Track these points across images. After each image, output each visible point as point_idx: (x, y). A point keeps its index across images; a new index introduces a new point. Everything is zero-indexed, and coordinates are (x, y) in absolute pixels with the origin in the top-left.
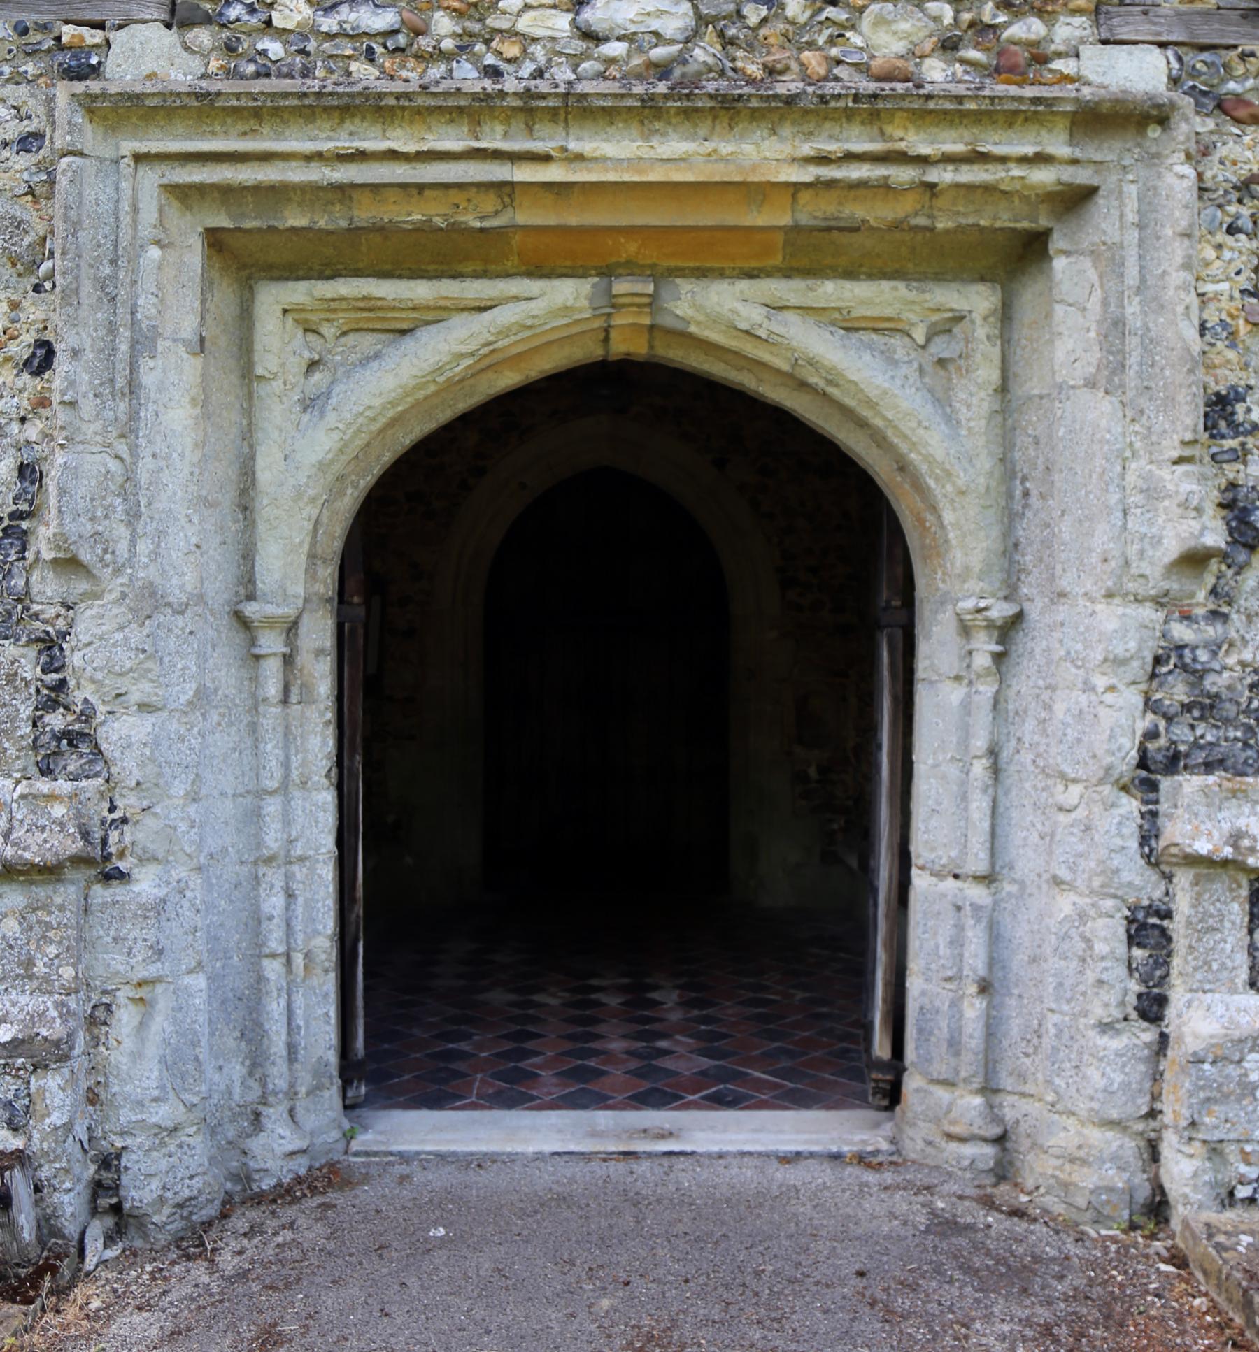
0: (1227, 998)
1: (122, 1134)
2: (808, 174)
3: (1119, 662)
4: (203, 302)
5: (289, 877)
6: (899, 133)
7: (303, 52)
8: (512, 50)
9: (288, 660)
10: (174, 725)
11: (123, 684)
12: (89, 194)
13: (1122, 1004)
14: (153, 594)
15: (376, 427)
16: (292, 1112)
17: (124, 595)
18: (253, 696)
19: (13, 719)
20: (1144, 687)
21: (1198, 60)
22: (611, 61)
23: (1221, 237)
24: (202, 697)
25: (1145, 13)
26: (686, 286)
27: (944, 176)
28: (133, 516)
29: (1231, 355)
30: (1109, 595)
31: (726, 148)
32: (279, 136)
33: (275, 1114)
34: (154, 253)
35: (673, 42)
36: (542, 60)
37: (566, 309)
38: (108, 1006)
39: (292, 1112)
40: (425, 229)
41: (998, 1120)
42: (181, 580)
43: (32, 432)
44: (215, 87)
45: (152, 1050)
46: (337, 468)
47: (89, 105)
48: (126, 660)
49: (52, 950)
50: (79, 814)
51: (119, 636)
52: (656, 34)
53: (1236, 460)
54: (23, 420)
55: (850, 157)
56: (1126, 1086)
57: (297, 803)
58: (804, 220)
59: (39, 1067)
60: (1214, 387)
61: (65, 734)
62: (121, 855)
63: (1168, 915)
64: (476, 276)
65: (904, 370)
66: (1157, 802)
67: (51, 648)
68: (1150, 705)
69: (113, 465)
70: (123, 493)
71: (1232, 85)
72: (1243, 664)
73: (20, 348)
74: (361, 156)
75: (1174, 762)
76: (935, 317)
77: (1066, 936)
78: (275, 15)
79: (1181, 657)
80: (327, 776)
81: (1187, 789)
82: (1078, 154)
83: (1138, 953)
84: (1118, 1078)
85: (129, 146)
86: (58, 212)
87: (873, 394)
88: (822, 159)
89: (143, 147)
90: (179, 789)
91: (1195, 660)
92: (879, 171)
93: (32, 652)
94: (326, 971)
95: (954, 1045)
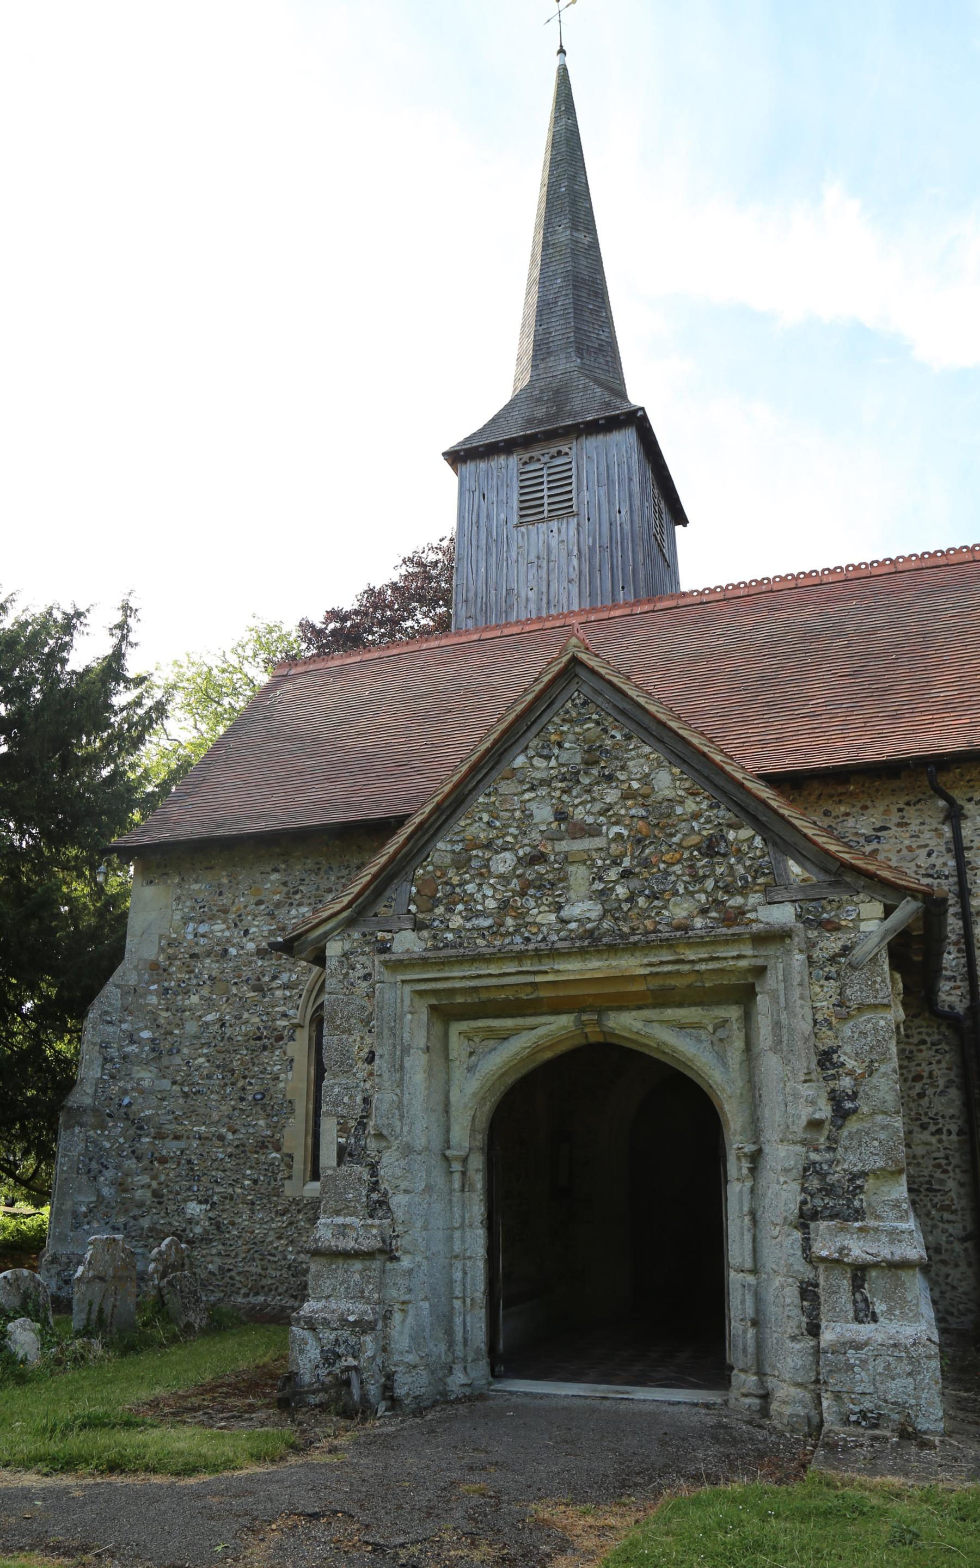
0: (843, 1325)
1: (395, 1365)
2: (647, 971)
3: (786, 1171)
4: (428, 1033)
5: (464, 1265)
6: (682, 951)
7: (459, 937)
8: (535, 930)
9: (464, 1173)
10: (417, 1199)
11: (398, 1182)
12: (386, 996)
13: (799, 1327)
14: (409, 1147)
15: (495, 1078)
16: (465, 1368)
17: (398, 1148)
18: (450, 1188)
19: (360, 1195)
20: (800, 1181)
21: (810, 906)
22: (571, 931)
23: (822, 982)
24: (429, 1188)
25: (786, 888)
26: (612, 1014)
27: (703, 967)
28: (402, 1117)
29: (829, 1033)
30: (782, 1141)
31: (614, 963)
32: (451, 971)
33: (457, 1367)
34: (409, 1016)
35: (595, 921)
36: (545, 932)
37: (564, 1027)
38: (391, 1311)
39: (465, 1368)
40: (506, 1000)
41: (765, 1388)
42: (420, 1142)
43: (368, 1086)
44: (429, 954)
45: (407, 1331)
46: (481, 1094)
47: (385, 963)
48: (399, 1173)
49: (371, 1287)
50: (382, 1233)
51: (397, 1163)
52: (588, 918)
53: (835, 1079)
54: (365, 1081)
55: (662, 963)
56: (804, 1366)
57: (468, 1233)
58: (651, 987)
59: (364, 1332)
60: (821, 1048)
61: (378, 1201)
62: (397, 1250)
63: (817, 1285)
64: (531, 1015)
65: (705, 1044)
66: (809, 1233)
67: (373, 1168)
68: (804, 1190)
69: (395, 1098)
70: (398, 1108)
71: (825, 915)
72: (845, 1170)
73: (364, 1054)
74: (479, 976)
75: (815, 1215)
76: (716, 1021)
77: (777, 1296)
78: (450, 924)
79: (815, 1168)
80: (482, 1223)
81: (821, 1227)
82: (756, 953)
83: (805, 1303)
84: (800, 1363)
85: (400, 978)
86: (375, 1003)
87: (690, 1056)
88: (651, 965)
89: (404, 978)
90: (419, 1224)
91: (821, 1169)
92: (676, 967)
93: (367, 1169)
94: (481, 1308)
95: (745, 1350)
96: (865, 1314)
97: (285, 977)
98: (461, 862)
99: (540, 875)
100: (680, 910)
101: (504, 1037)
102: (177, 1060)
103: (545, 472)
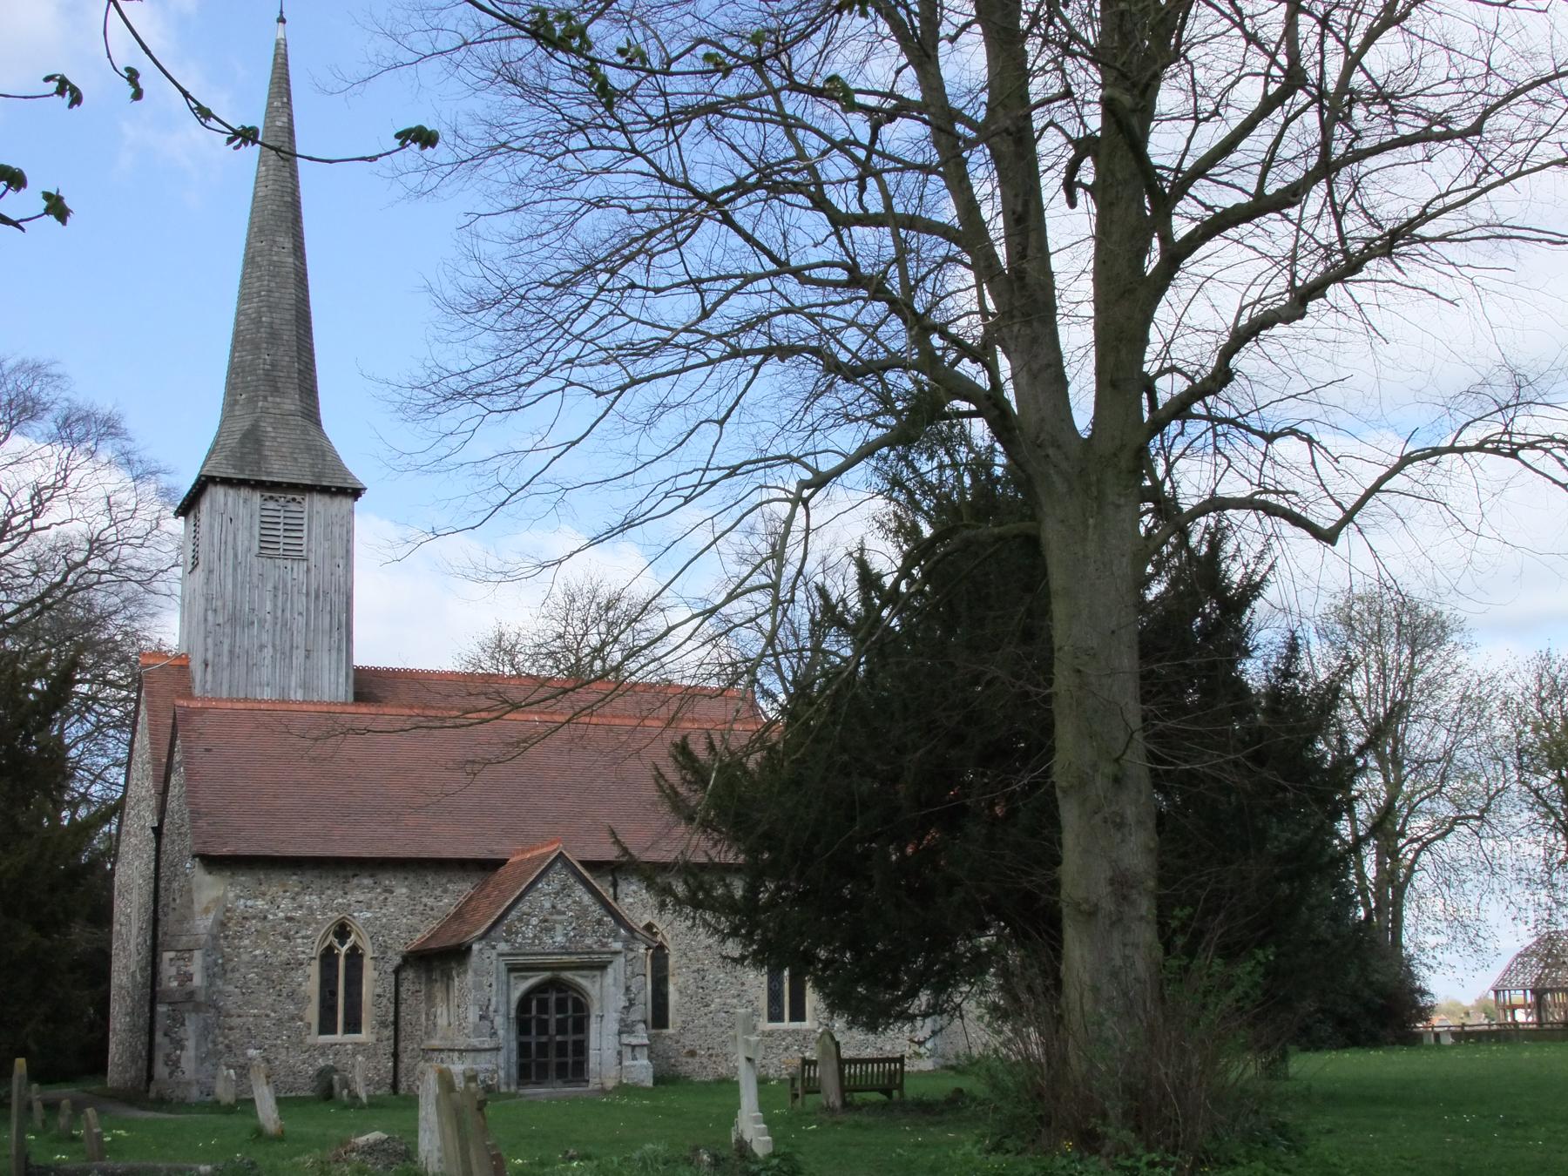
96: (634, 1058)
97: (303, 933)
98: (520, 920)
99: (547, 927)
100: (588, 941)
101: (526, 978)
102: (237, 975)
103: (281, 514)
